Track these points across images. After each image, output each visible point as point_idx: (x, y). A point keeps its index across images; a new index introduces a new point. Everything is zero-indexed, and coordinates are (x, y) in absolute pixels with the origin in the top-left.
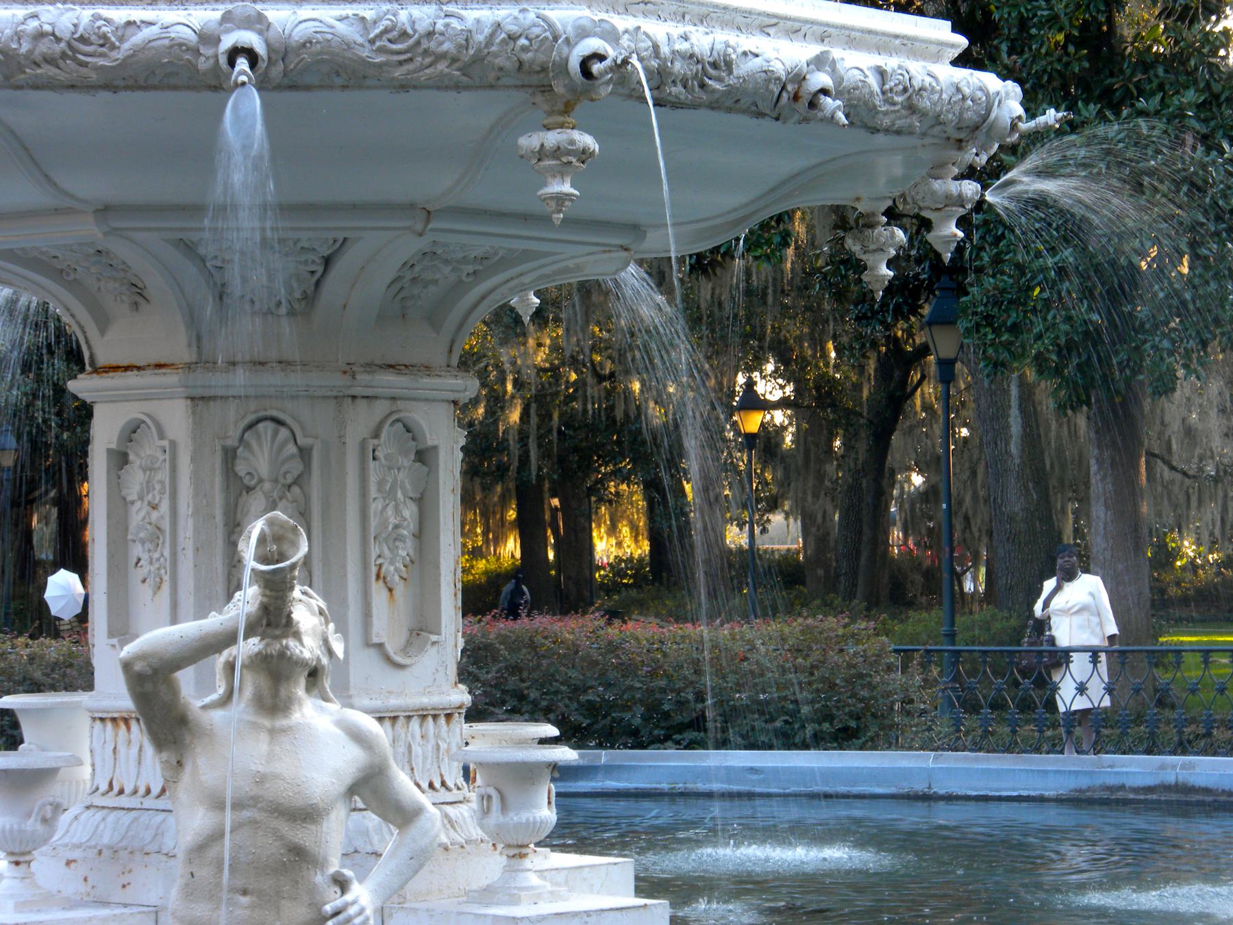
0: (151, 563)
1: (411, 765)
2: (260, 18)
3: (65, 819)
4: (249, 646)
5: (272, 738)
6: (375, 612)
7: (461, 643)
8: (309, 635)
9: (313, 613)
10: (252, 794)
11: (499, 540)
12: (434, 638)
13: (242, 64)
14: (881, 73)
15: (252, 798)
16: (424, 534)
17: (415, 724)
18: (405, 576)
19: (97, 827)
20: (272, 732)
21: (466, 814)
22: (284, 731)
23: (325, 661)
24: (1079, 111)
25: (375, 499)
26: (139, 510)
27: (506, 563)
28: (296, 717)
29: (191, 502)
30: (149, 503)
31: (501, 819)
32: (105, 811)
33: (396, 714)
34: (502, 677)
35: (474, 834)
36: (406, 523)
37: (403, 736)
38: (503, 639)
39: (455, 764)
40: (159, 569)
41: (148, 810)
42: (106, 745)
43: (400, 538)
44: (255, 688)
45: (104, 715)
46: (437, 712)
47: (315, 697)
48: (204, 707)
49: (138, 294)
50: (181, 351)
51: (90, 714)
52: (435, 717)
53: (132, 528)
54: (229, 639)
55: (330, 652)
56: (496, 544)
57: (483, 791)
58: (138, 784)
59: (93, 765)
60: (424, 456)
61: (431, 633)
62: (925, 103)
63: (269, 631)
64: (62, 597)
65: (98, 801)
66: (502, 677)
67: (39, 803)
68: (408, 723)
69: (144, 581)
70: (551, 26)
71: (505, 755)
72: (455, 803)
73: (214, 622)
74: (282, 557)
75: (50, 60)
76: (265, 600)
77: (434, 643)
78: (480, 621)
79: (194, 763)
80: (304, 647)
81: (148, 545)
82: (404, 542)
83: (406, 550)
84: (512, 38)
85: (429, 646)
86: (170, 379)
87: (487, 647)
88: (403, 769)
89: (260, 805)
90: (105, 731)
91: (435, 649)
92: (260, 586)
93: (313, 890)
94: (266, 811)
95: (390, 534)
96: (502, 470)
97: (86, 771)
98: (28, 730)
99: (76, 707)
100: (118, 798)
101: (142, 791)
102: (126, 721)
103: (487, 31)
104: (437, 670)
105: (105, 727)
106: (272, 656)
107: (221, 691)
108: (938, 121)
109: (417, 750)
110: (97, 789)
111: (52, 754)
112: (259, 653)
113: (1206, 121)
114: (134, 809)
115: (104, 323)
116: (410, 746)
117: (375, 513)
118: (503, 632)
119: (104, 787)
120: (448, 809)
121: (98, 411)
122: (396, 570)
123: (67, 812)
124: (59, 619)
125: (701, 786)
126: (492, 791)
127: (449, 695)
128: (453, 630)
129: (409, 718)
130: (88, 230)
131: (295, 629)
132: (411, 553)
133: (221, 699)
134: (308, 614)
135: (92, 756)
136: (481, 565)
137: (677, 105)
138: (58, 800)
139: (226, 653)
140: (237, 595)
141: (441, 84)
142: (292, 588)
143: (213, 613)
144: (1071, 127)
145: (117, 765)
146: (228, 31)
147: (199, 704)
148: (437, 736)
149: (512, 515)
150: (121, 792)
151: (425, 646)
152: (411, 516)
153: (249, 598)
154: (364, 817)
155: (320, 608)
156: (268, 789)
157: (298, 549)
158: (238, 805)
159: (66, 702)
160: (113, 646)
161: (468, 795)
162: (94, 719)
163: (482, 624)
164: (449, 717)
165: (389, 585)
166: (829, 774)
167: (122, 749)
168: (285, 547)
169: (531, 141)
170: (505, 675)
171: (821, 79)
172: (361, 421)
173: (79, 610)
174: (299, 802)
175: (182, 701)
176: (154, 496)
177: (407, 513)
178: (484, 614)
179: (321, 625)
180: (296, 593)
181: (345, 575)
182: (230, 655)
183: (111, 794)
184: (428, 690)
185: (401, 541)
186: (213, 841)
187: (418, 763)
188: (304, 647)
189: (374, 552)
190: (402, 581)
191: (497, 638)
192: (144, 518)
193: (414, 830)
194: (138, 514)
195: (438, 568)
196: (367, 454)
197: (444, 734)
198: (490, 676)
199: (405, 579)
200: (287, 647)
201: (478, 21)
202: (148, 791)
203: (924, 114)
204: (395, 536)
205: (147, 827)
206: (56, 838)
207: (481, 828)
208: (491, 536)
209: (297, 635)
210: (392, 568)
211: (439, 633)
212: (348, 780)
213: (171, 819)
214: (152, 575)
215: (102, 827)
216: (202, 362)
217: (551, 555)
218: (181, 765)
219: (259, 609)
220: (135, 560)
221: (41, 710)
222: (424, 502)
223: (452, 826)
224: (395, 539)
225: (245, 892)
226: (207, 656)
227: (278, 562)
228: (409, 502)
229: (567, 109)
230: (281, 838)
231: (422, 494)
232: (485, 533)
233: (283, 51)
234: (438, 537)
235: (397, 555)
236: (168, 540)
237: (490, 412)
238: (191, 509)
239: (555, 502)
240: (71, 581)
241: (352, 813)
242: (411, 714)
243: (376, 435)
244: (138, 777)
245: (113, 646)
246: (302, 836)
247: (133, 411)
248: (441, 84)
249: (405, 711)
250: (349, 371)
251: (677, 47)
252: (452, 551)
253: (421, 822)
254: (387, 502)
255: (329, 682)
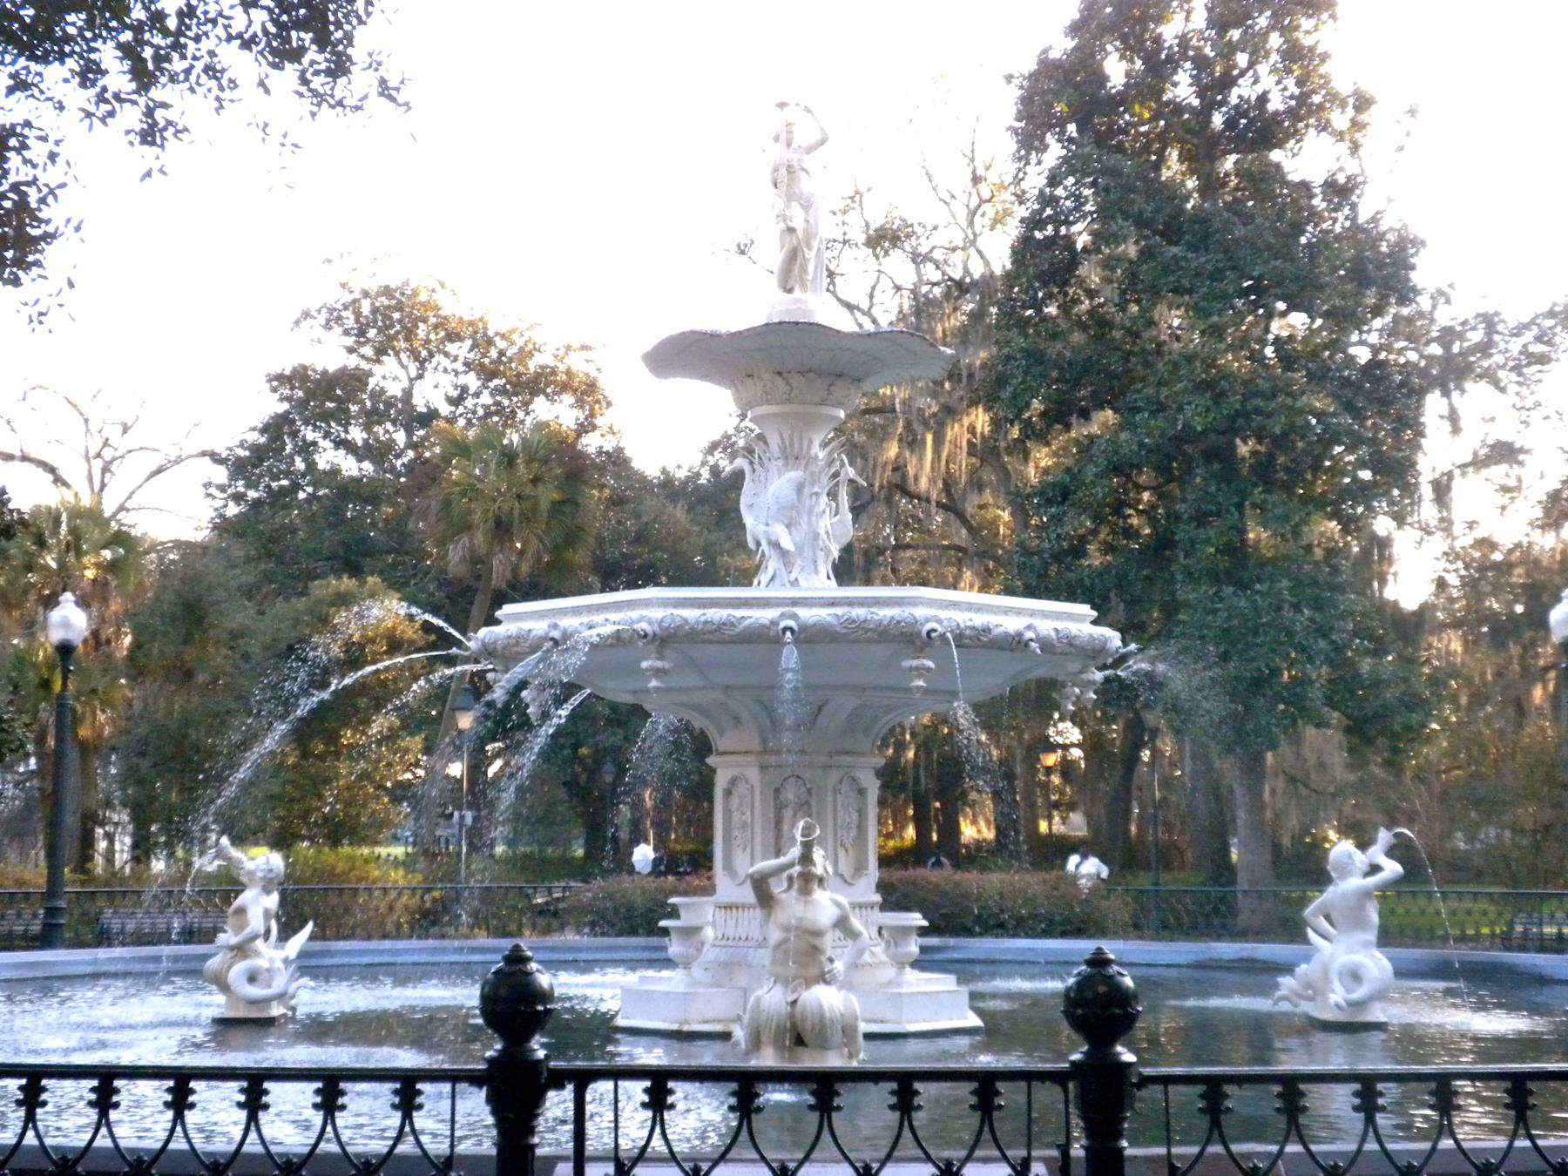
4: (798, 868)
11: (903, 828)
13: (788, 634)
14: (1057, 631)
16: (861, 827)
27: (908, 843)
38: (900, 880)
49: (737, 721)
50: (755, 745)
54: (791, 865)
60: (862, 792)
62: (1077, 642)
73: (782, 860)
75: (710, 632)
83: (853, 833)
86: (751, 758)
96: (903, 786)
98: (683, 913)
108: (1083, 649)
113: (1295, 596)
115: (722, 732)
121: (719, 771)
125: (998, 957)
130: (717, 695)
136: (891, 843)
137: (967, 647)
141: (869, 641)
144: (1140, 650)
149: (911, 812)
153: (795, 852)
166: (1062, 951)
169: (906, 664)
171: (1030, 635)
172: (834, 776)
193: (858, 942)
194: (736, 816)
196: (836, 791)
203: (1076, 647)
216: (765, 751)
217: (935, 837)
222: (862, 813)
229: (922, 650)
232: (894, 824)
233: (804, 628)
237: (896, 751)
239: (938, 805)
243: (841, 782)
246: (817, 942)
247: (735, 772)
248: (869, 641)
250: (830, 755)
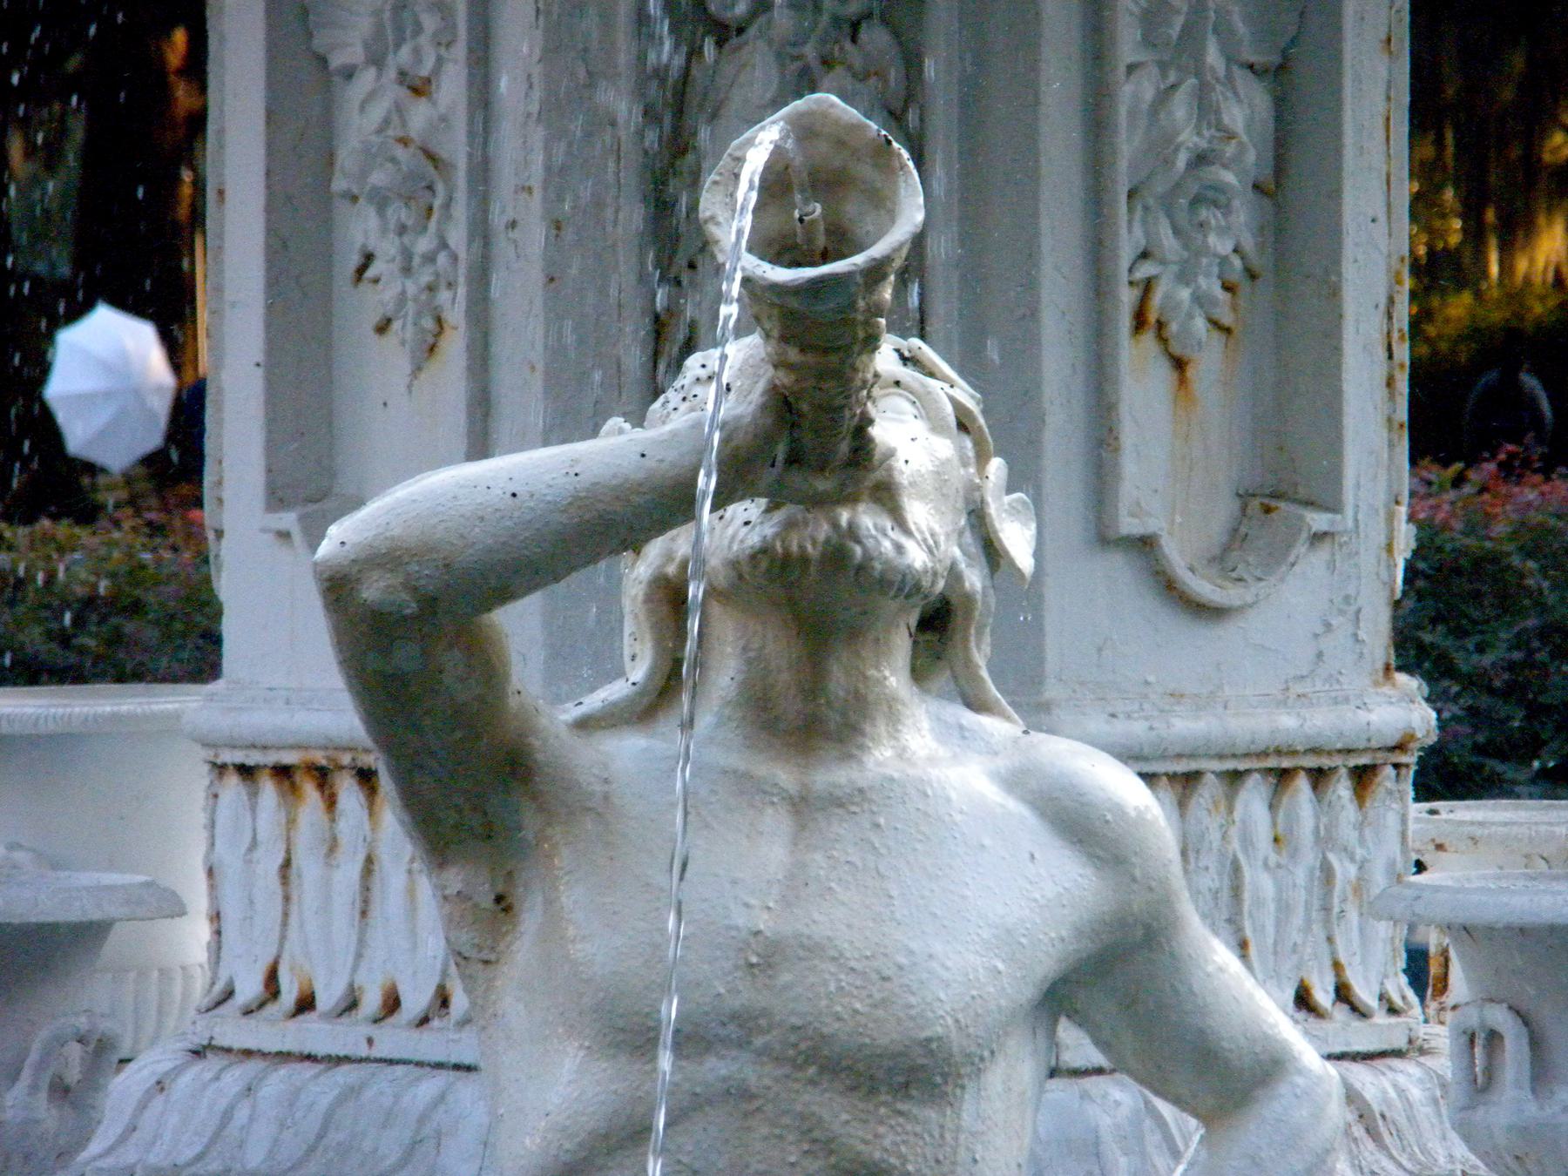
0: (407, 270)
1: (1239, 930)
3: (125, 1087)
5: (802, 827)
6: (1128, 436)
7: (1406, 539)
8: (922, 497)
9: (937, 427)
10: (737, 1003)
12: (1318, 521)
15: (734, 1016)
17: (1253, 798)
18: (1227, 319)
19: (227, 1116)
20: (803, 807)
21: (1416, 1093)
22: (838, 802)
23: (974, 579)
24: (915, 1117)
25: (1131, 68)
26: (371, 96)
28: (880, 758)
29: (537, 71)
30: (402, 74)
31: (1532, 1109)
32: (254, 1066)
33: (1193, 766)
34: (1529, 663)
35: (1442, 1160)
36: (1230, 150)
37: (1215, 836)
39: (1383, 929)
40: (431, 288)
41: (391, 1062)
42: (258, 854)
43: (1211, 197)
44: (749, 662)
45: (253, 758)
46: (1325, 762)
47: (941, 696)
48: (584, 725)
51: (209, 754)
52: (1319, 777)
53: (347, 157)
55: (992, 552)
56: (1506, 250)
57: (1472, 1018)
58: (360, 979)
59: (216, 917)
61: (1310, 504)
63: (796, 479)
64: (108, 395)
65: (233, 1031)
66: (1529, 663)
67: (44, 1034)
68: (1230, 799)
69: (383, 328)
71: (1546, 901)
72: (1383, 1054)
74: (840, 242)
76: (785, 378)
77: (1318, 538)
78: (1458, 481)
79: (549, 902)
80: (907, 532)
81: (398, 212)
82: (1227, 210)
85: (1301, 548)
87: (1486, 566)
88: (1216, 933)
89: (759, 1042)
90: (253, 809)
91: (1323, 553)
92: (767, 336)
94: (778, 1060)
95: (1178, 185)
97: (194, 936)
99: (170, 727)
100: (292, 1025)
101: (372, 1001)
102: (322, 776)
104: (1328, 626)
105: (254, 795)
106: (804, 560)
107: (639, 671)
109: (1260, 883)
110: (229, 994)
111: (86, 878)
112: (765, 550)
114: (347, 1059)
116: (1236, 869)
117: (1132, 114)
118: (1535, 517)
119: (250, 988)
120: (1361, 1075)
122: (1198, 299)
123: (132, 1066)
124: (91, 468)
126: (1500, 1018)
127: (1364, 706)
128: (1382, 497)
129: (1235, 778)
131: (879, 475)
132: (1248, 244)
133: (630, 701)
134: (920, 427)
135: (212, 888)
138: (105, 1026)
139: (655, 549)
140: (693, 362)
142: (871, 343)
143: (616, 422)
145: (293, 920)
147: (570, 713)
148: (1325, 840)
150: (306, 1004)
151: (1289, 547)
152: (1249, 126)
154: (1085, 1096)
155: (958, 407)
156: (787, 987)
157: (892, 217)
158: (691, 1041)
159: (132, 717)
160: (284, 535)
161: (1422, 1031)
162: (220, 769)
163: (1467, 489)
164: (1363, 777)
165: (1176, 349)
167: (308, 866)
168: (851, 208)
170: (1542, 656)
173: (153, 439)
174: (887, 1035)
175: (513, 702)
176: (417, 51)
177: (1235, 116)
178: (1472, 461)
179: (965, 464)
180: (885, 360)
181: (1033, 313)
182: (669, 557)
183: (272, 1009)
184: (1298, 688)
185: (1216, 204)
186: (610, 1153)
187: (1261, 924)
188: (907, 532)
189: (1126, 246)
190: (1216, 335)
191: (1514, 536)
192: (386, 122)
195: (1335, 293)
197: (1348, 834)
198: (1487, 659)
199: (1228, 331)
200: (853, 533)
202: (392, 1003)
204: (1194, 188)
205: (388, 1119)
206: (95, 1147)
207: (1467, 1138)
208: (1490, 215)
209: (886, 496)
210: (1185, 294)
211: (1334, 507)
212: (1045, 964)
213: (466, 1091)
214: (411, 307)
215: (242, 1114)
218: (507, 909)
219: (763, 407)
220: (355, 260)
221: (51, 737)
223: (1373, 1133)
224: (1196, 201)
226: (593, 559)
227: (825, 258)
228: (1241, 77)
231: (1284, 53)
234: (1336, 194)
235: (1204, 250)
236: (461, 195)
238: (537, 94)
240: (130, 344)
241: (1056, 1084)
242: (1242, 766)
244: (359, 956)
245: (284, 535)
249: (1221, 757)
252: (1383, 244)
253: (1277, 1106)
254: (1172, 77)
255: (987, 648)
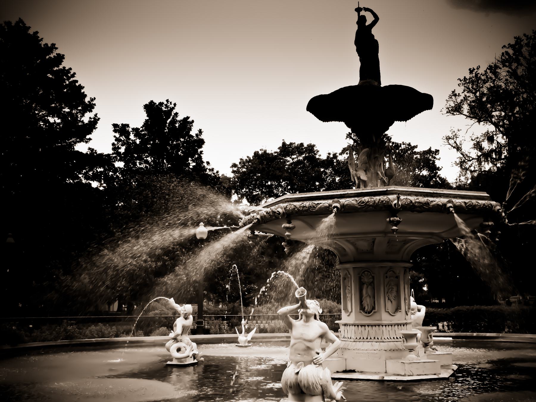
2: (339, 201)
13: (335, 209)
14: (465, 203)
52: (401, 325)
70: (389, 199)
84: (382, 201)
93: (311, 355)
103: (378, 200)
129: (395, 325)
146: (333, 204)
201: (376, 199)
225: (299, 354)
230: (305, 345)
251: (416, 201)
